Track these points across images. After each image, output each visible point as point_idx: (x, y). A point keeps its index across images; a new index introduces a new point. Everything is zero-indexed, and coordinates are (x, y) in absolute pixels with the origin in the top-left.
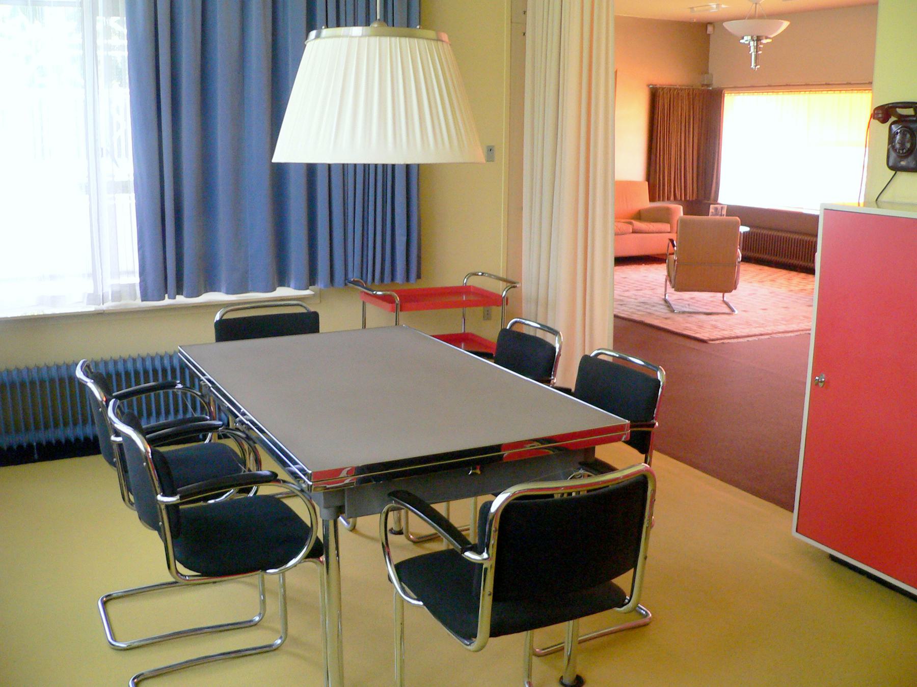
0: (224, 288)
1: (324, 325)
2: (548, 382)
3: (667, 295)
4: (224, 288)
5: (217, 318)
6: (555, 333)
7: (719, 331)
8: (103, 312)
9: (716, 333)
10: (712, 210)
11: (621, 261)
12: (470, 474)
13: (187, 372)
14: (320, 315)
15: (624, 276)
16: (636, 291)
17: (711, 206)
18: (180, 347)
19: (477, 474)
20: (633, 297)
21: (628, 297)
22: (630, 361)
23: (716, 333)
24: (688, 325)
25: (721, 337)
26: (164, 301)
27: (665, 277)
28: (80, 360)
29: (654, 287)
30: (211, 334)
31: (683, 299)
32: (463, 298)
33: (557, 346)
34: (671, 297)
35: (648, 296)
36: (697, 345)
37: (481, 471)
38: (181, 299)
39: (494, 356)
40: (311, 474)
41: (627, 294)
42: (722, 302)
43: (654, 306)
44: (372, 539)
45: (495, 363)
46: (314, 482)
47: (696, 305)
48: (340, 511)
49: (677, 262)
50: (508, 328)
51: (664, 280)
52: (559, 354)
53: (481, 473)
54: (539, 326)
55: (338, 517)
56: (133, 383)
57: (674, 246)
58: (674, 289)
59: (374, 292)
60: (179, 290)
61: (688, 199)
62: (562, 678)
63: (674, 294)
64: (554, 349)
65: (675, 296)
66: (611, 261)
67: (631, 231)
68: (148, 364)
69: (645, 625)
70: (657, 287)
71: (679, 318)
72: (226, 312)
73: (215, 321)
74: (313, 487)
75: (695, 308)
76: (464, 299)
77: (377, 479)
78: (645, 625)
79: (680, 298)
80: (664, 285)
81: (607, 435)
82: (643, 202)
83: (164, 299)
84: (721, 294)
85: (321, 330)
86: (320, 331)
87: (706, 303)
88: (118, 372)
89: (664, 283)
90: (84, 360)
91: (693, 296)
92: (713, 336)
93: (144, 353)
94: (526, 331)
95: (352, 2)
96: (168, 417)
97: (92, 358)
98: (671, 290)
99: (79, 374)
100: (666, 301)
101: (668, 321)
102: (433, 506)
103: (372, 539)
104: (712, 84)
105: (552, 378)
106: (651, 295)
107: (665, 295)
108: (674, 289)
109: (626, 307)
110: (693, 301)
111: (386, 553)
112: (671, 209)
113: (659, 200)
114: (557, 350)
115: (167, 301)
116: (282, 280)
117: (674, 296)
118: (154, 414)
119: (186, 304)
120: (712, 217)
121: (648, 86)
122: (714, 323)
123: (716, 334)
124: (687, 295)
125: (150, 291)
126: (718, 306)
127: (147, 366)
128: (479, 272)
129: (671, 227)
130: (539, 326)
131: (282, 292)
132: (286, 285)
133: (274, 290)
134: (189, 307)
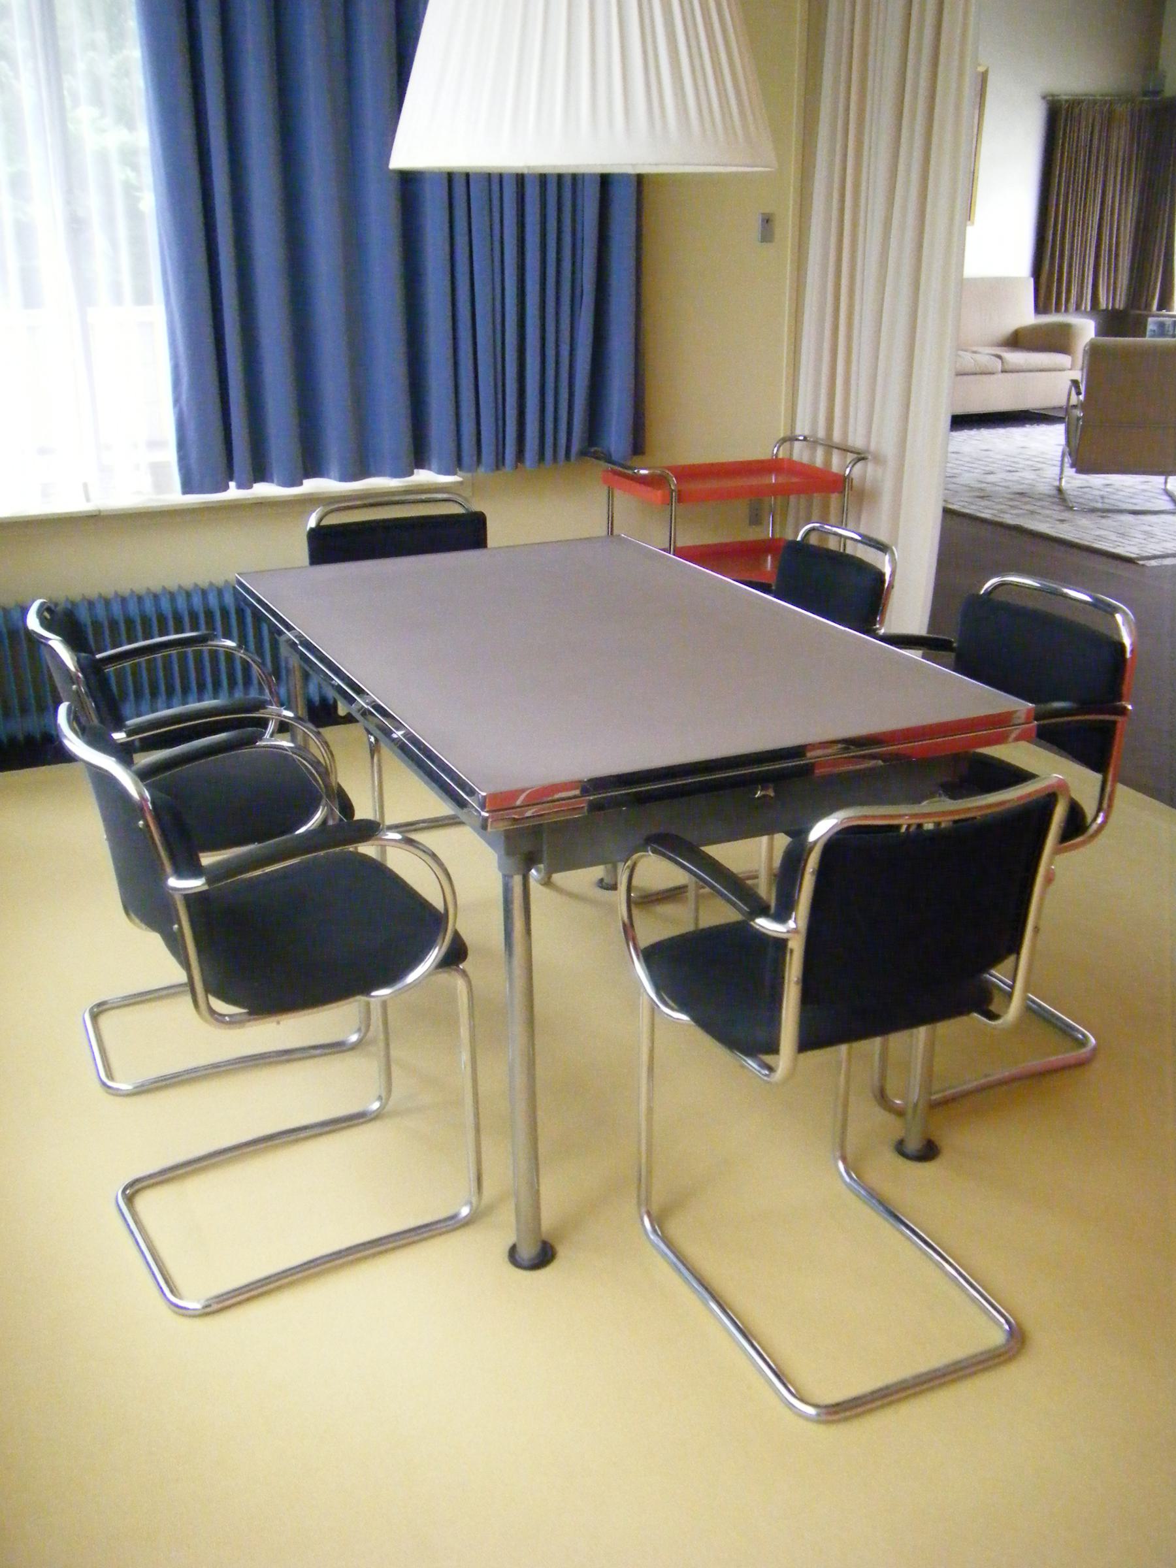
0: (334, 467)
1: (495, 533)
2: (870, 632)
3: (1063, 480)
4: (334, 468)
5: (312, 523)
6: (882, 547)
7: (1158, 543)
8: (98, 513)
9: (1151, 546)
10: (1151, 324)
11: (961, 422)
12: (757, 796)
13: (248, 613)
14: (484, 512)
15: (985, 448)
16: (1008, 474)
17: (1150, 320)
18: (238, 574)
19: (770, 796)
20: (1001, 484)
21: (994, 484)
22: (1066, 596)
23: (1151, 546)
24: (1102, 532)
25: (1159, 553)
26: (228, 491)
27: (1060, 449)
28: (33, 601)
29: (1040, 466)
30: (301, 551)
31: (1090, 487)
32: (772, 479)
33: (887, 571)
34: (1069, 483)
35: (1026, 482)
36: (1122, 570)
37: (775, 791)
38: (263, 490)
39: (774, 588)
40: (484, 797)
41: (990, 478)
42: (1162, 491)
43: (1040, 500)
44: (697, 919)
45: (775, 597)
46: (495, 811)
47: (1115, 497)
48: (530, 860)
49: (1083, 422)
50: (799, 539)
51: (1060, 454)
52: (891, 586)
53: (775, 796)
54: (859, 538)
55: (531, 870)
56: (124, 637)
57: (1079, 393)
58: (1074, 470)
59: (636, 471)
60: (260, 473)
61: (1103, 306)
62: (900, 1149)
63: (1075, 479)
64: (881, 575)
65: (1077, 481)
66: (946, 421)
67: (1000, 370)
68: (149, 607)
69: (1081, 1064)
70: (1044, 465)
71: (1084, 521)
72: (332, 511)
73: (308, 529)
74: (490, 820)
75: (1112, 502)
76: (773, 481)
77: (616, 803)
78: (1081, 1064)
79: (1086, 485)
80: (1059, 463)
81: (997, 725)
82: (1024, 314)
83: (226, 488)
84: (1161, 479)
85: (491, 542)
86: (489, 546)
87: (1133, 493)
88: (146, 616)
89: (1060, 459)
90: (41, 600)
91: (1108, 482)
92: (1146, 552)
93: (172, 585)
94: (832, 544)
95: (386, 10)
96: (218, 692)
97: (131, 590)
98: (1070, 472)
99: (33, 623)
100: (1060, 490)
101: (1065, 526)
102: (703, 848)
103: (697, 919)
104: (1163, 91)
105: (878, 626)
106: (1033, 480)
107: (1061, 479)
108: (1074, 470)
109: (989, 500)
110: (1108, 490)
111: (630, 937)
112: (1075, 325)
113: (1058, 310)
114: (887, 578)
115: (233, 492)
116: (420, 459)
117: (1074, 481)
118: (147, 691)
119: (263, 498)
120: (1149, 339)
121: (1044, 98)
122: (1149, 528)
123: (1153, 548)
124: (1097, 480)
125: (196, 477)
126: (1153, 497)
127: (179, 606)
128: (800, 436)
129: (1073, 361)
130: (859, 538)
131: (423, 476)
132: (426, 467)
133: (411, 474)
134: (1050, 408)
